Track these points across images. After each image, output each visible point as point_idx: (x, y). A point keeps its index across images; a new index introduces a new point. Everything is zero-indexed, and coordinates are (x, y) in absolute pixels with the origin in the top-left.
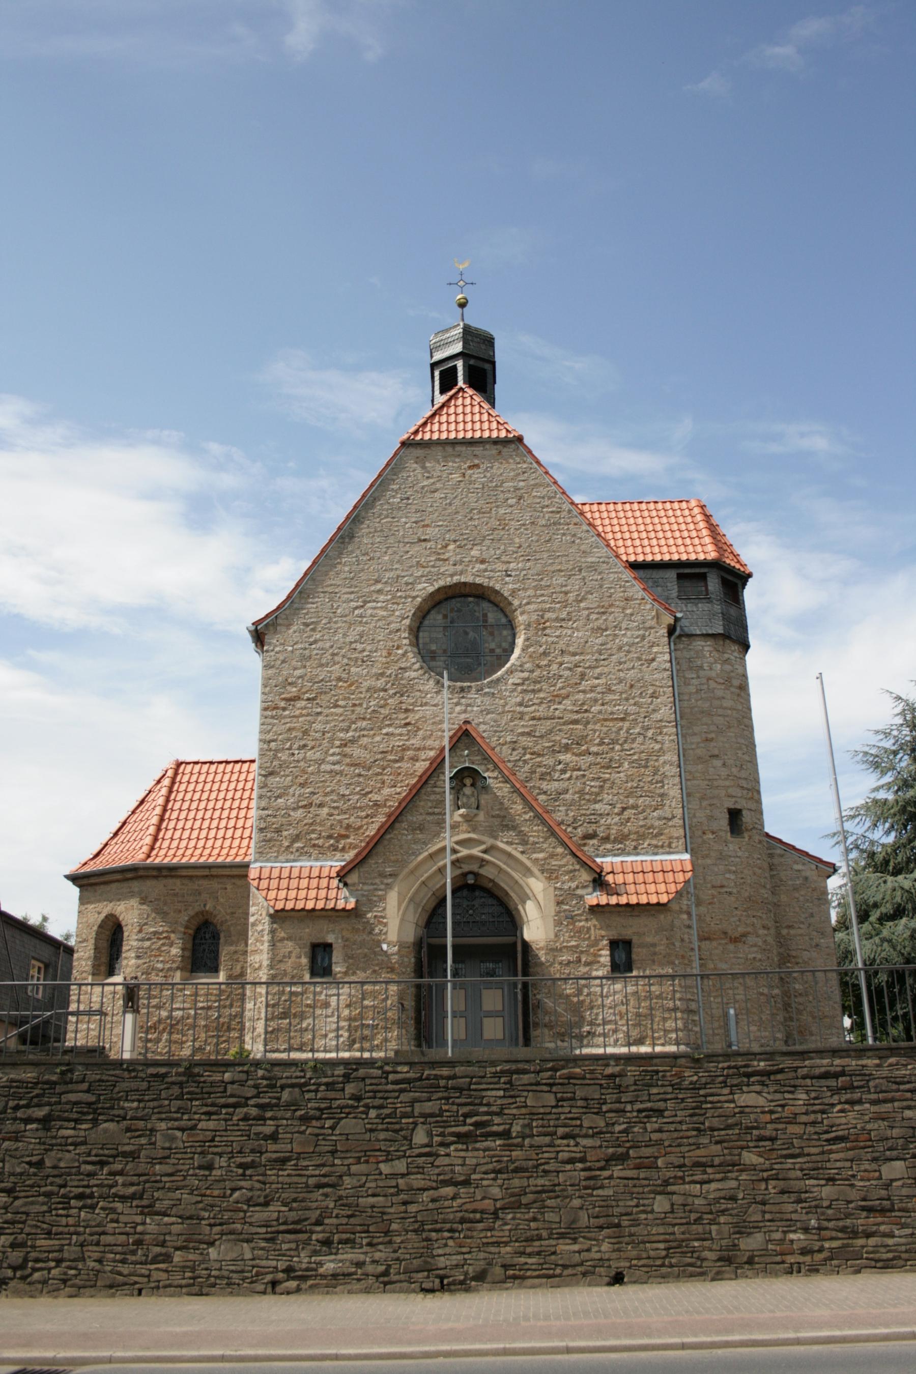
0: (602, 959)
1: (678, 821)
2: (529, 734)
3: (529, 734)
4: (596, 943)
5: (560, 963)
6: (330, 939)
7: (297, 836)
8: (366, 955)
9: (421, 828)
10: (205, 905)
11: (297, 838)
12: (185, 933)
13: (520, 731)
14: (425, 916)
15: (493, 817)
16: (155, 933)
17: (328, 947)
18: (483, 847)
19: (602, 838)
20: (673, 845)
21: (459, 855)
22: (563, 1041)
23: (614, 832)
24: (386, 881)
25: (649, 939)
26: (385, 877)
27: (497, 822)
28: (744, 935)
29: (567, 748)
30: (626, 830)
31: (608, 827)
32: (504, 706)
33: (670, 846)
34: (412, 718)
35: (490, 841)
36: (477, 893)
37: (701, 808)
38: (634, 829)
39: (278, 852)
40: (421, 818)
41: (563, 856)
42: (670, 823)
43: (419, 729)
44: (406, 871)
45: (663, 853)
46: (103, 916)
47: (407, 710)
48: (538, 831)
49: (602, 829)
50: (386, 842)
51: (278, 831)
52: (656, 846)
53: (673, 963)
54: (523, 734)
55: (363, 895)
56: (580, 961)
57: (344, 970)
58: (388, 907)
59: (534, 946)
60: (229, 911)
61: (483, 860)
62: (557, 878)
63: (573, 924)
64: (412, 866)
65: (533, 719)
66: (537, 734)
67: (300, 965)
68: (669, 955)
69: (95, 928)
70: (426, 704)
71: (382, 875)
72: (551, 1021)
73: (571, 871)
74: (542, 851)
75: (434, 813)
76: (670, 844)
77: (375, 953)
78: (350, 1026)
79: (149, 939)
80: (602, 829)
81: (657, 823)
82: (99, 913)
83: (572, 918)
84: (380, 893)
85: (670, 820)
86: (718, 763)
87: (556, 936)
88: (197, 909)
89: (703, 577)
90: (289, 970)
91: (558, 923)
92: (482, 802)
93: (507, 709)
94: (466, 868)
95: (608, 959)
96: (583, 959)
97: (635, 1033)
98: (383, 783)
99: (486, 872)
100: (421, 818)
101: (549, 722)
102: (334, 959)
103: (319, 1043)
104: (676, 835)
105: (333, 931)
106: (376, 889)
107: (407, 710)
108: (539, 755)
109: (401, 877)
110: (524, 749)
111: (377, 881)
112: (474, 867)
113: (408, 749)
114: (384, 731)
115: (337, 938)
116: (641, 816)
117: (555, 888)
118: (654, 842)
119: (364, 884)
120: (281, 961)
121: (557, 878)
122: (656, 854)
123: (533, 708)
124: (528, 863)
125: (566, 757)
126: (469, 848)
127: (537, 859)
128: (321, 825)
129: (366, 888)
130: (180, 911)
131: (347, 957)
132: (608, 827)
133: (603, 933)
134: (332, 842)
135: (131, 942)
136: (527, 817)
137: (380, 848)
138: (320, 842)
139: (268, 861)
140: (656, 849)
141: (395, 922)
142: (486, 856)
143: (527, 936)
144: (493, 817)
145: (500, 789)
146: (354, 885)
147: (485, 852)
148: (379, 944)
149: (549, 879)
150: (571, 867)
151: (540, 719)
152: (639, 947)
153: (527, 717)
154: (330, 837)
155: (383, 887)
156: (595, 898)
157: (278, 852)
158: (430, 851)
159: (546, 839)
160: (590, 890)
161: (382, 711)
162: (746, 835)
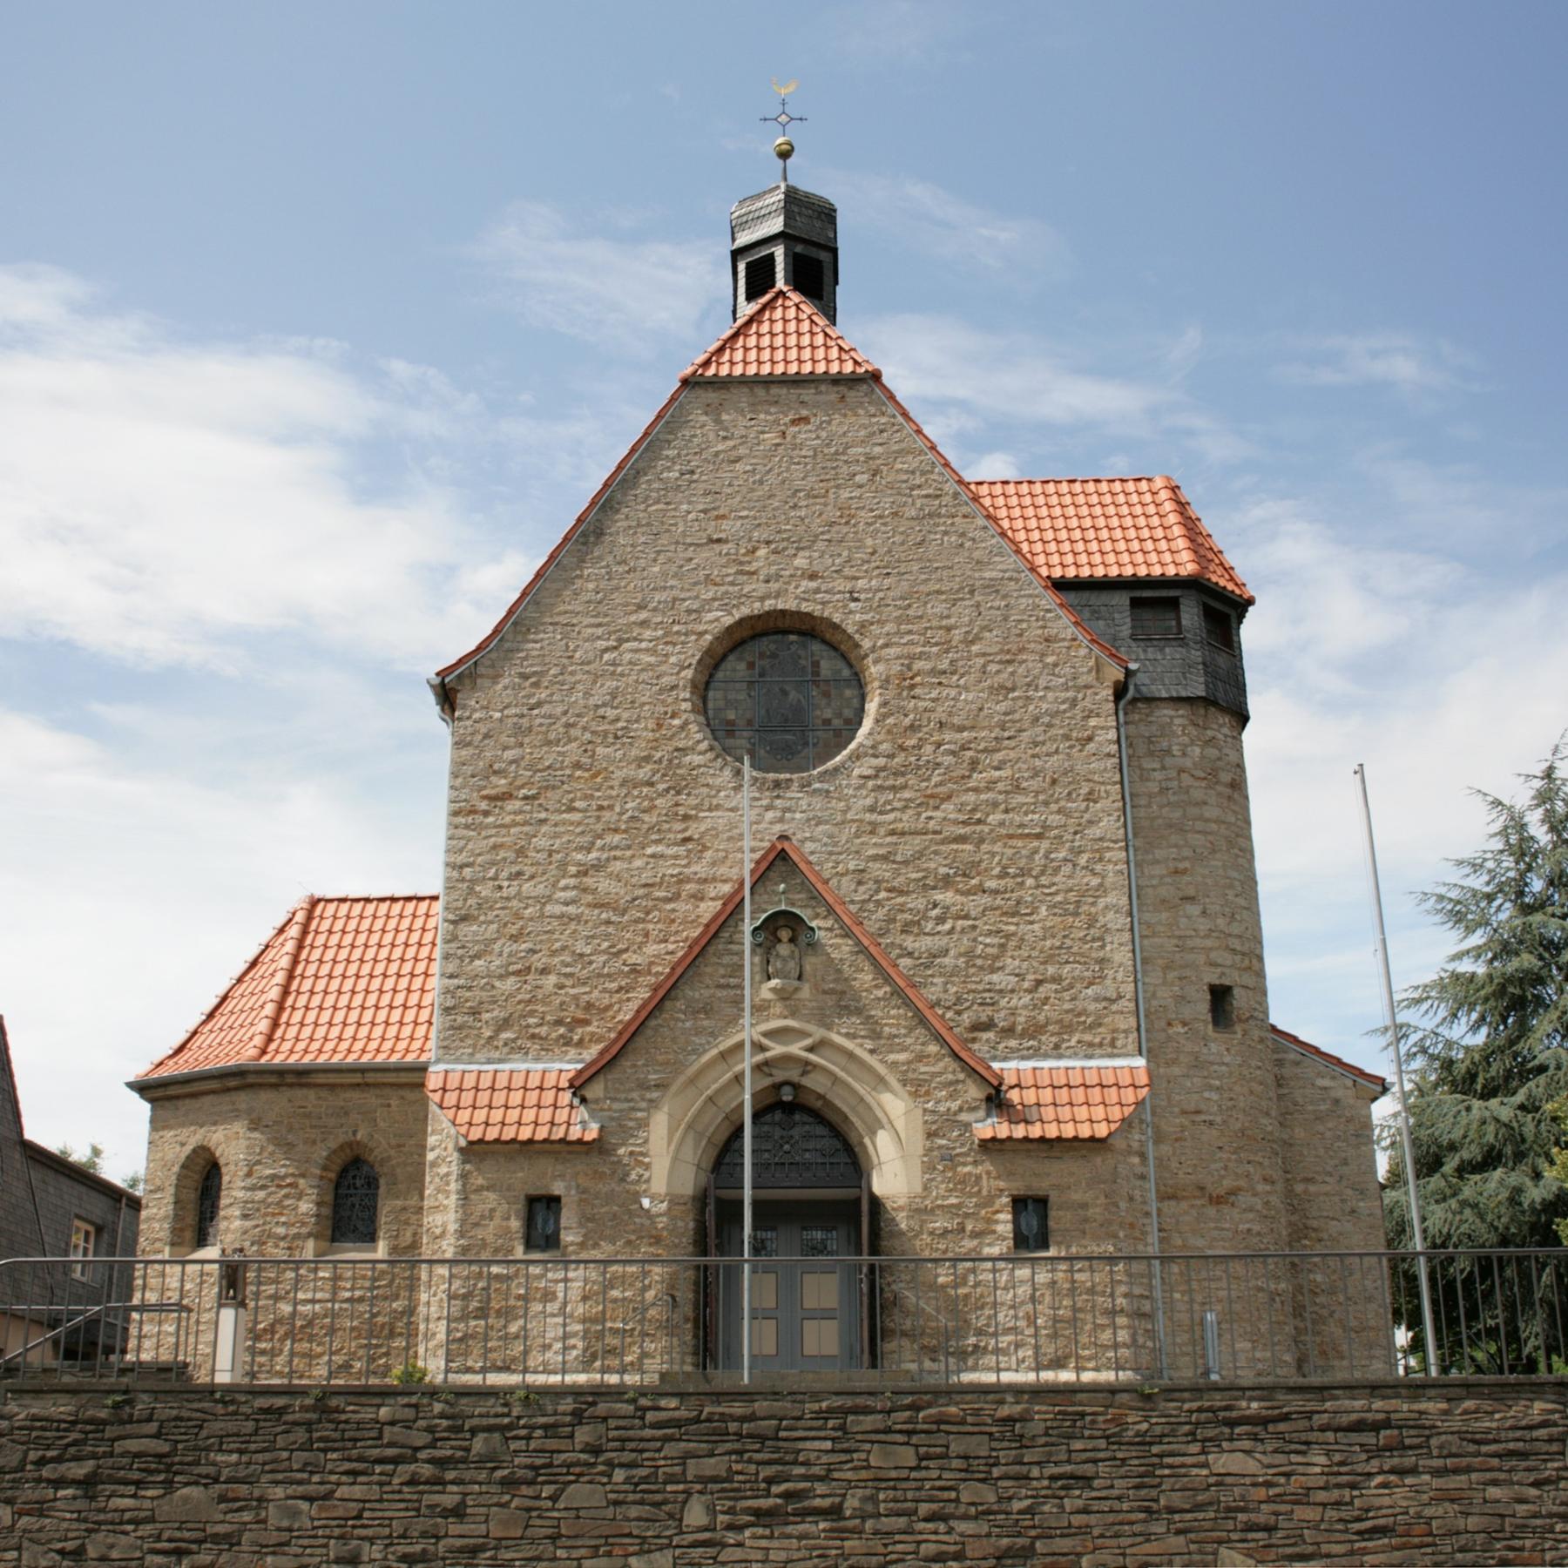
0: (1000, 1228)
1: (1126, 1004)
2: (884, 858)
3: (884, 858)
4: (989, 1201)
5: (931, 1233)
6: (557, 1188)
7: (506, 1020)
9: (707, 1010)
10: (355, 1133)
11: (505, 1024)
12: (321, 1178)
13: (871, 852)
15: (825, 992)
16: (273, 1177)
17: (553, 1202)
18: (808, 1042)
19: (1003, 1030)
20: (1119, 1043)
21: (768, 1054)
22: (933, 1360)
23: (1022, 1019)
24: (648, 1096)
25: (1076, 1196)
26: (648, 1088)
27: (831, 1001)
28: (1233, 1192)
29: (946, 882)
30: (1041, 1018)
31: (1013, 1012)
32: (845, 812)
33: (1113, 1044)
34: (694, 830)
35: (819, 1033)
36: (797, 1117)
37: (1164, 983)
38: (1054, 1016)
39: (474, 1046)
40: (706, 993)
41: (938, 1058)
42: (1114, 1007)
43: (705, 848)
44: (682, 1079)
45: (1102, 1056)
46: (188, 1149)
47: (686, 817)
48: (898, 1017)
49: (1002, 1014)
50: (649, 1032)
51: (475, 1013)
52: (1091, 1045)
53: (1115, 1236)
54: (875, 858)
55: (612, 1119)
56: (963, 1230)
57: (579, 1239)
59: (889, 1205)
60: (393, 1142)
61: (807, 1063)
62: (927, 1093)
63: (953, 1168)
65: (892, 833)
66: (899, 858)
67: (508, 1231)
69: (176, 1169)
70: (718, 807)
71: (643, 1086)
73: (951, 1083)
74: (904, 1049)
75: (728, 986)
76: (1113, 1040)
78: (586, 1331)
79: (263, 1187)
80: (1002, 1014)
81: (1092, 1007)
82: (183, 1145)
83: (951, 1160)
84: (639, 1114)
85: (1113, 1001)
86: (1194, 910)
87: (925, 1188)
88: (341, 1139)
89: (1174, 604)
90: (490, 1239)
91: (929, 1168)
92: (808, 968)
93: (849, 816)
94: (780, 1075)
95: (1010, 1227)
96: (969, 1227)
97: (1049, 1350)
98: (647, 935)
99: (813, 1082)
100: (706, 993)
101: (918, 840)
104: (1122, 1027)
105: (562, 1176)
106: (633, 1109)
107: (686, 817)
108: (902, 893)
109: (674, 1088)
110: (877, 882)
111: (635, 1095)
112: (793, 1074)
113: (688, 880)
114: (649, 851)
115: (568, 1188)
117: (925, 1110)
118: (1088, 1037)
119: (613, 1099)
120: (476, 1225)
121: (927, 1093)
122: (1090, 1057)
123: (891, 816)
124: (882, 1069)
125: (946, 897)
128: (544, 1003)
129: (616, 1106)
130: (314, 1142)
131: (585, 1219)
132: (1013, 1012)
133: (1002, 1184)
134: (562, 1030)
135: (234, 1192)
136: (880, 993)
138: (543, 1031)
139: (458, 1061)
141: (664, 1164)
142: (812, 1057)
144: (825, 992)
145: (837, 947)
146: (597, 1101)
147: (811, 1049)
148: (636, 1197)
149: (915, 1095)
150: (950, 1077)
151: (903, 834)
153: (882, 831)
154: (559, 1022)
155: (644, 1105)
156: (989, 1127)
157: (474, 1046)
158: (722, 1048)
159: (911, 1030)
160: (981, 1113)
161: (646, 817)
162: (1238, 1028)
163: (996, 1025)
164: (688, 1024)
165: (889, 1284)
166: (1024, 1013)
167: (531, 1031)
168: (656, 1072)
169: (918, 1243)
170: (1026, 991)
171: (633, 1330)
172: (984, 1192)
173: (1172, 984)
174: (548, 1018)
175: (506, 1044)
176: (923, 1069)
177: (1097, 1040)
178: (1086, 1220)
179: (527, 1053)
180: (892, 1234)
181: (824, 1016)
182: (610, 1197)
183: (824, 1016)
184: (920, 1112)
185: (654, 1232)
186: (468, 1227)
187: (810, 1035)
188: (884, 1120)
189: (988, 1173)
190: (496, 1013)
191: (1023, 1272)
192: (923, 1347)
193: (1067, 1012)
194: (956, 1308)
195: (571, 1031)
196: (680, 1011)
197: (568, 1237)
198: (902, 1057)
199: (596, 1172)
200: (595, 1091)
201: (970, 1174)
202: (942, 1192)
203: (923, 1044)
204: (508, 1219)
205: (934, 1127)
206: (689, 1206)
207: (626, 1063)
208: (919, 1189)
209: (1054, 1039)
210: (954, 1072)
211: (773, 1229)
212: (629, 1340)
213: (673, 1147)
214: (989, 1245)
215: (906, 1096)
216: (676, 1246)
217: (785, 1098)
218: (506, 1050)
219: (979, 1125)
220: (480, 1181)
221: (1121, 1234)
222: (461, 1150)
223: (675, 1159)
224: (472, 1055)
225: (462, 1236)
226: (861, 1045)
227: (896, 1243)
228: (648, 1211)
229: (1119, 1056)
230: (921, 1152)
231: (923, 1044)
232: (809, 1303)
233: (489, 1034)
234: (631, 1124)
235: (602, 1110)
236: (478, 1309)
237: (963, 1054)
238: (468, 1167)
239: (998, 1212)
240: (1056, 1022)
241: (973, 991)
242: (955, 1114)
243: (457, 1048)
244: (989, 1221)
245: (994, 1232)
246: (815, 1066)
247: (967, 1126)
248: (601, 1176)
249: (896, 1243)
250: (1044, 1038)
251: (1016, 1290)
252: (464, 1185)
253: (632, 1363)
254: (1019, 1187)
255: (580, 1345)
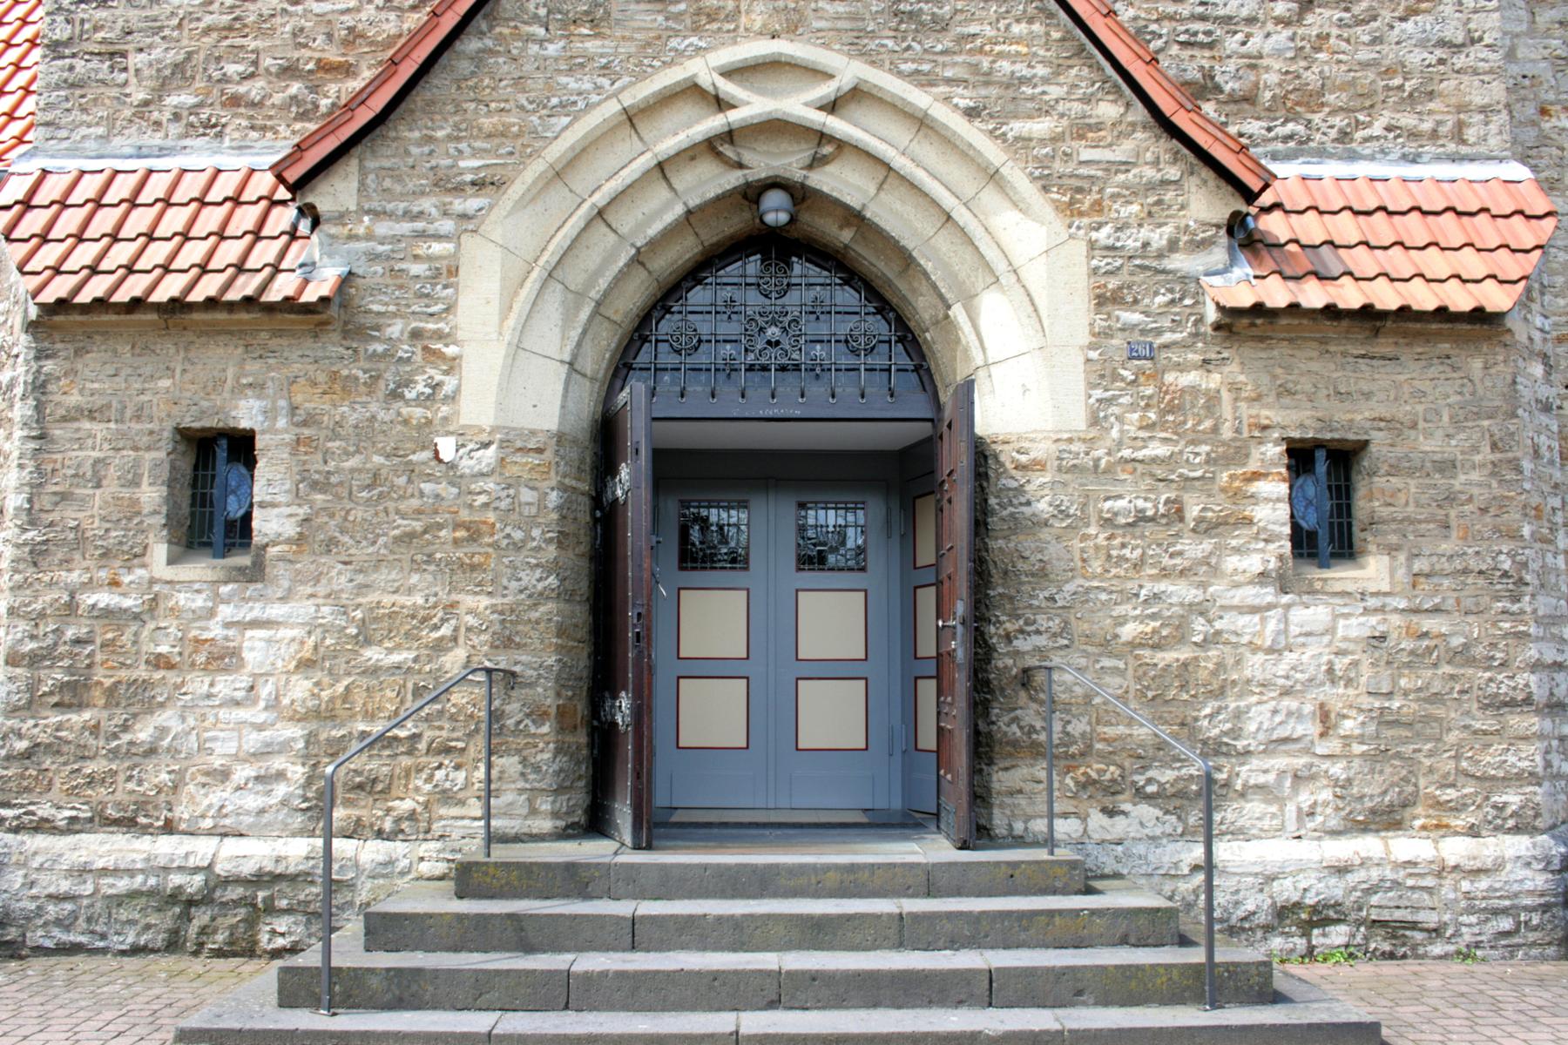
0: (1261, 513)
4: (1236, 453)
5: (1107, 522)
6: (245, 414)
7: (178, 67)
8: (376, 478)
11: (179, 73)
14: (606, 342)
17: (242, 446)
18: (826, 90)
19: (1233, 99)
20: (1471, 134)
21: (734, 116)
22: (1111, 812)
23: (1272, 78)
24: (459, 205)
25: (1430, 445)
26: (458, 189)
30: (1312, 77)
31: (1253, 63)
33: (1458, 135)
35: (849, 71)
36: (798, 267)
37: (1532, 32)
38: (1338, 73)
39: (111, 121)
41: (1121, 131)
42: (1460, 61)
44: (536, 168)
45: (1438, 158)
49: (1231, 66)
50: (465, 66)
51: (114, 55)
52: (1413, 135)
53: (1514, 535)
55: (374, 257)
56: (1180, 515)
57: (290, 529)
58: (465, 302)
59: (1007, 455)
61: (822, 137)
62: (1098, 207)
63: (1156, 376)
64: (556, 151)
67: (133, 510)
68: (1502, 504)
71: (447, 184)
72: (1068, 739)
73: (1151, 187)
74: (1044, 111)
76: (1460, 126)
77: (411, 470)
78: (310, 739)
80: (1231, 66)
81: (1416, 58)
83: (1144, 352)
84: (437, 248)
85: (1456, 48)
87: (1095, 421)
90: (95, 527)
91: (1102, 375)
94: (762, 162)
95: (1284, 511)
96: (1193, 511)
97: (1374, 789)
99: (842, 182)
102: (260, 492)
103: (195, 802)
104: (1478, 100)
105: (258, 387)
106: (422, 235)
109: (516, 190)
111: (427, 204)
112: (789, 162)
115: (270, 414)
116: (1363, 34)
117: (1092, 245)
118: (1407, 120)
119: (377, 214)
120: (64, 497)
121: (1098, 207)
122: (1414, 159)
124: (993, 153)
126: (773, 94)
127: (1024, 140)
128: (261, 33)
129: (383, 228)
131: (310, 483)
132: (1253, 63)
133: (1267, 414)
134: (295, 88)
137: (439, 81)
138: (254, 89)
139: (73, 152)
140: (1413, 146)
141: (503, 363)
142: (836, 125)
143: (985, 423)
146: (341, 218)
147: (832, 107)
148: (423, 436)
149: (1070, 210)
150: (1150, 173)
152: (1394, 470)
154: (289, 71)
155: (447, 226)
156: (1241, 285)
157: (111, 121)
158: (628, 99)
159: (1058, 70)
160: (1219, 255)
163: (1218, 89)
164: (552, 49)
165: (1008, 638)
166: (1277, 65)
167: (231, 89)
168: (476, 153)
169: (1077, 544)
170: (1279, 21)
171: (415, 737)
172: (1227, 433)
173: (1547, 34)
174: (267, 62)
175: (176, 117)
176: (1086, 155)
177: (1427, 126)
178: (1451, 498)
179: (220, 135)
180: (1017, 525)
181: (862, 33)
182: (366, 434)
183: (862, 33)
184: (1082, 247)
185: (465, 515)
186: (46, 502)
187: (829, 76)
188: (1000, 266)
189: (1235, 388)
190: (157, 53)
191: (1311, 615)
192: (1087, 784)
193: (1365, 65)
194: (1169, 693)
195: (314, 89)
196: (536, 19)
197: (265, 524)
198: (1041, 127)
199: (334, 377)
200: (335, 194)
201: (1194, 390)
202: (1132, 430)
203: (1086, 100)
204: (135, 483)
205: (1113, 283)
206: (548, 455)
207: (407, 133)
208: (1078, 421)
209: (1339, 121)
210: (1156, 163)
211: (743, 505)
212: (406, 761)
213: (511, 322)
214: (1237, 550)
215: (1049, 212)
216: (518, 547)
217: (770, 218)
218: (175, 129)
219: (1216, 281)
220: (74, 399)
221: (1526, 531)
222: (32, 327)
223: (518, 347)
224: (105, 138)
225: (33, 523)
226: (947, 99)
227: (1026, 544)
228: (452, 466)
229: (1472, 159)
230: (1086, 339)
231: (1086, 100)
232: (809, 648)
233: (141, 95)
234: (417, 269)
235: (352, 237)
236: (63, 686)
237: (1182, 120)
238: (49, 366)
239: (1256, 476)
240: (1342, 88)
241: (1171, 18)
242: (1160, 255)
243: (75, 126)
244: (1237, 495)
245: (1249, 522)
246: (841, 145)
247: (1188, 285)
248: (341, 386)
249: (1026, 544)
250: (1317, 118)
251: (1302, 651)
252: (39, 408)
253: (412, 816)
254: (1301, 421)
255: (298, 772)
